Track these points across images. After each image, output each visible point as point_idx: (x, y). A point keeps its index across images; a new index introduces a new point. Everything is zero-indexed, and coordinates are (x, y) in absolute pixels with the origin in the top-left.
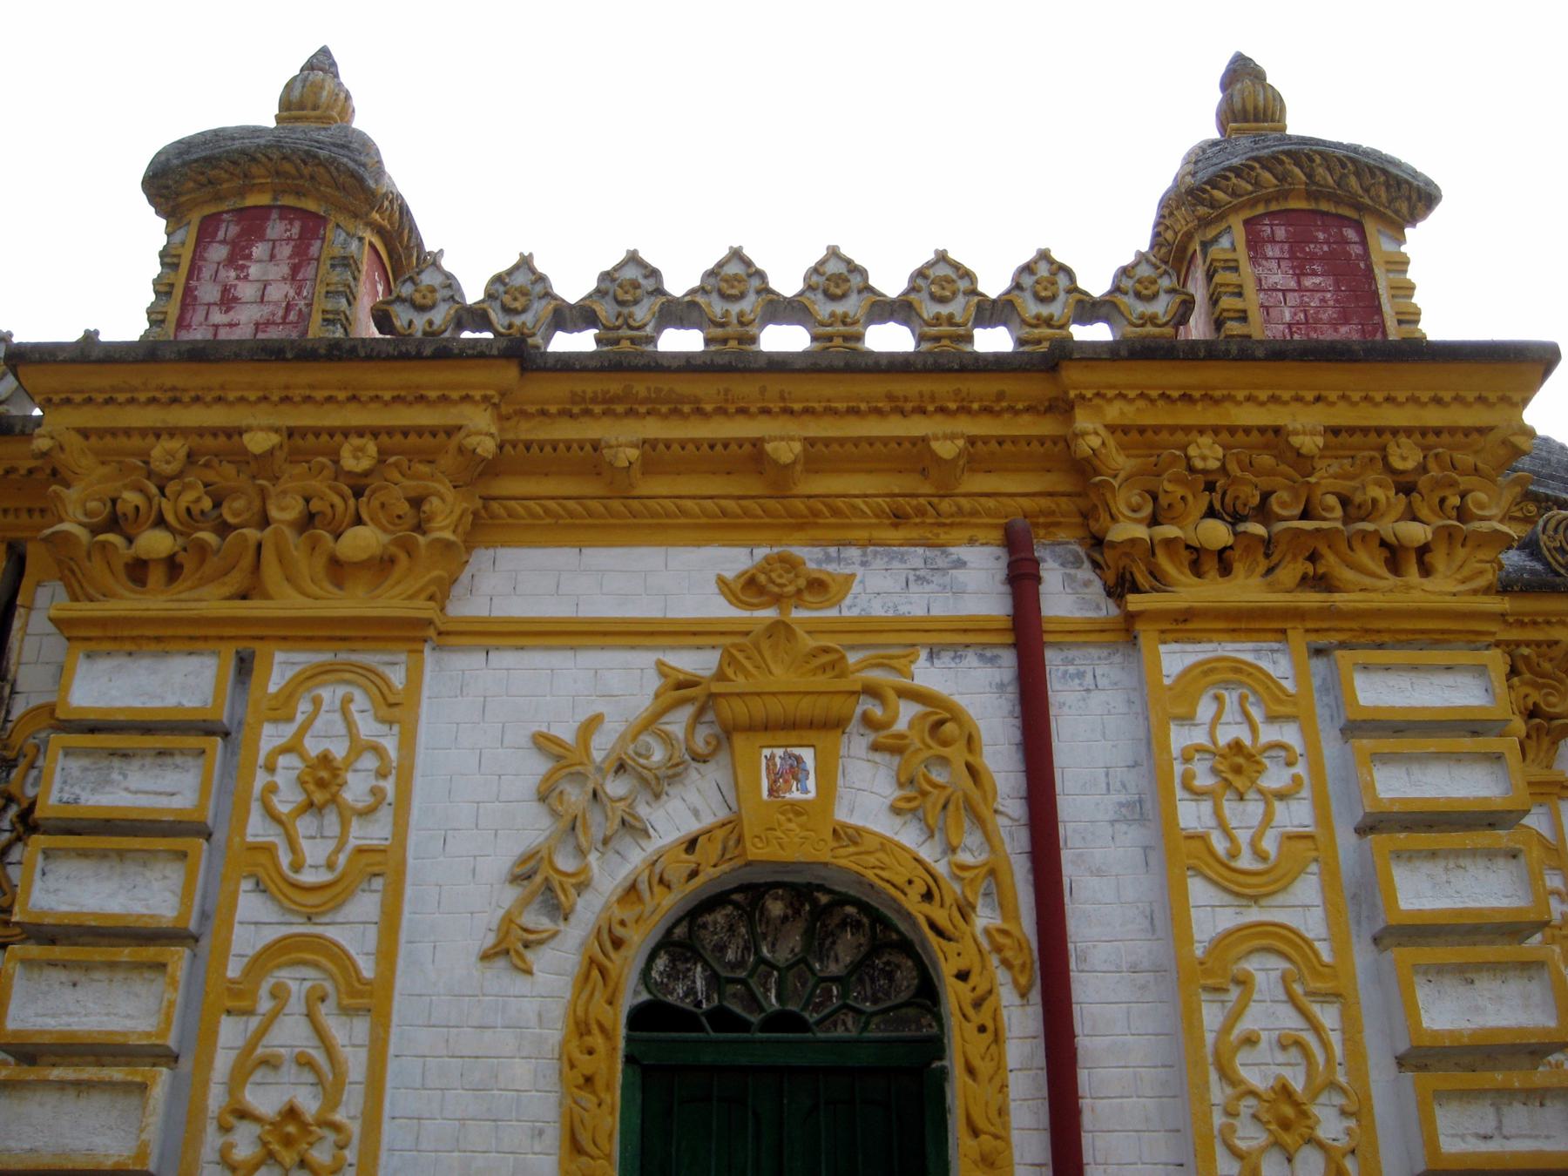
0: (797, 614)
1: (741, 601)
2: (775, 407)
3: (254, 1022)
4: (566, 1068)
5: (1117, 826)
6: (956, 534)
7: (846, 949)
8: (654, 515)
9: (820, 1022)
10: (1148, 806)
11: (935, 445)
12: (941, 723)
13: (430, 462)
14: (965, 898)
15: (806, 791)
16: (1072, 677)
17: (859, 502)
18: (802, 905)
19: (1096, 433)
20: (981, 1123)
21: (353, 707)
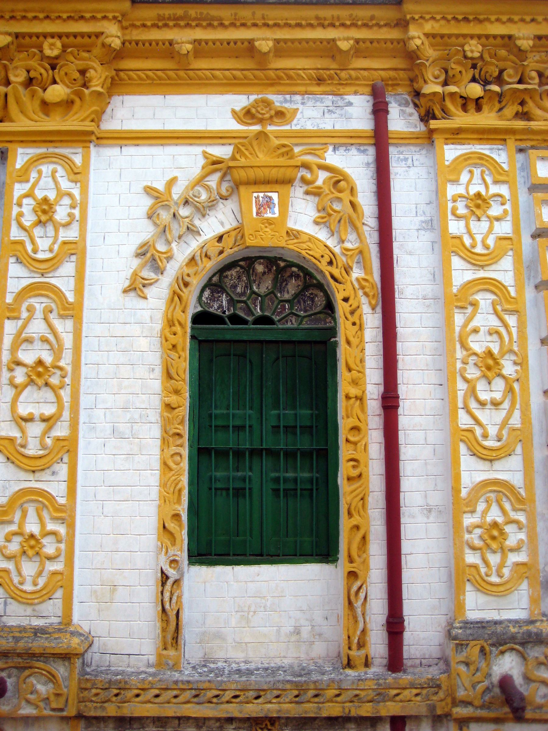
0: (270, 128)
1: (243, 122)
2: (260, 23)
3: (20, 323)
4: (164, 341)
5: (420, 231)
6: (348, 89)
7: (292, 288)
8: (200, 79)
9: (279, 321)
10: (435, 222)
11: (339, 43)
12: (339, 181)
13: (88, 51)
14: (348, 264)
15: (274, 213)
16: (402, 160)
17: (301, 72)
18: (272, 267)
19: (419, 38)
20: (352, 365)
21: (58, 175)
